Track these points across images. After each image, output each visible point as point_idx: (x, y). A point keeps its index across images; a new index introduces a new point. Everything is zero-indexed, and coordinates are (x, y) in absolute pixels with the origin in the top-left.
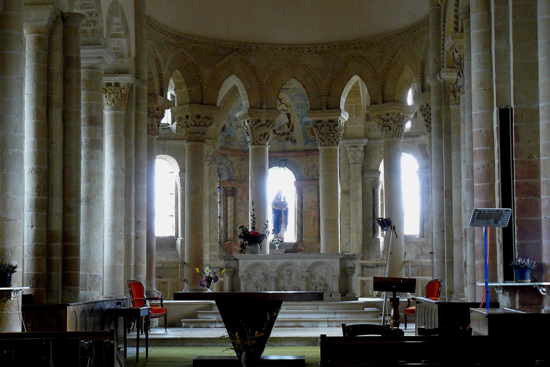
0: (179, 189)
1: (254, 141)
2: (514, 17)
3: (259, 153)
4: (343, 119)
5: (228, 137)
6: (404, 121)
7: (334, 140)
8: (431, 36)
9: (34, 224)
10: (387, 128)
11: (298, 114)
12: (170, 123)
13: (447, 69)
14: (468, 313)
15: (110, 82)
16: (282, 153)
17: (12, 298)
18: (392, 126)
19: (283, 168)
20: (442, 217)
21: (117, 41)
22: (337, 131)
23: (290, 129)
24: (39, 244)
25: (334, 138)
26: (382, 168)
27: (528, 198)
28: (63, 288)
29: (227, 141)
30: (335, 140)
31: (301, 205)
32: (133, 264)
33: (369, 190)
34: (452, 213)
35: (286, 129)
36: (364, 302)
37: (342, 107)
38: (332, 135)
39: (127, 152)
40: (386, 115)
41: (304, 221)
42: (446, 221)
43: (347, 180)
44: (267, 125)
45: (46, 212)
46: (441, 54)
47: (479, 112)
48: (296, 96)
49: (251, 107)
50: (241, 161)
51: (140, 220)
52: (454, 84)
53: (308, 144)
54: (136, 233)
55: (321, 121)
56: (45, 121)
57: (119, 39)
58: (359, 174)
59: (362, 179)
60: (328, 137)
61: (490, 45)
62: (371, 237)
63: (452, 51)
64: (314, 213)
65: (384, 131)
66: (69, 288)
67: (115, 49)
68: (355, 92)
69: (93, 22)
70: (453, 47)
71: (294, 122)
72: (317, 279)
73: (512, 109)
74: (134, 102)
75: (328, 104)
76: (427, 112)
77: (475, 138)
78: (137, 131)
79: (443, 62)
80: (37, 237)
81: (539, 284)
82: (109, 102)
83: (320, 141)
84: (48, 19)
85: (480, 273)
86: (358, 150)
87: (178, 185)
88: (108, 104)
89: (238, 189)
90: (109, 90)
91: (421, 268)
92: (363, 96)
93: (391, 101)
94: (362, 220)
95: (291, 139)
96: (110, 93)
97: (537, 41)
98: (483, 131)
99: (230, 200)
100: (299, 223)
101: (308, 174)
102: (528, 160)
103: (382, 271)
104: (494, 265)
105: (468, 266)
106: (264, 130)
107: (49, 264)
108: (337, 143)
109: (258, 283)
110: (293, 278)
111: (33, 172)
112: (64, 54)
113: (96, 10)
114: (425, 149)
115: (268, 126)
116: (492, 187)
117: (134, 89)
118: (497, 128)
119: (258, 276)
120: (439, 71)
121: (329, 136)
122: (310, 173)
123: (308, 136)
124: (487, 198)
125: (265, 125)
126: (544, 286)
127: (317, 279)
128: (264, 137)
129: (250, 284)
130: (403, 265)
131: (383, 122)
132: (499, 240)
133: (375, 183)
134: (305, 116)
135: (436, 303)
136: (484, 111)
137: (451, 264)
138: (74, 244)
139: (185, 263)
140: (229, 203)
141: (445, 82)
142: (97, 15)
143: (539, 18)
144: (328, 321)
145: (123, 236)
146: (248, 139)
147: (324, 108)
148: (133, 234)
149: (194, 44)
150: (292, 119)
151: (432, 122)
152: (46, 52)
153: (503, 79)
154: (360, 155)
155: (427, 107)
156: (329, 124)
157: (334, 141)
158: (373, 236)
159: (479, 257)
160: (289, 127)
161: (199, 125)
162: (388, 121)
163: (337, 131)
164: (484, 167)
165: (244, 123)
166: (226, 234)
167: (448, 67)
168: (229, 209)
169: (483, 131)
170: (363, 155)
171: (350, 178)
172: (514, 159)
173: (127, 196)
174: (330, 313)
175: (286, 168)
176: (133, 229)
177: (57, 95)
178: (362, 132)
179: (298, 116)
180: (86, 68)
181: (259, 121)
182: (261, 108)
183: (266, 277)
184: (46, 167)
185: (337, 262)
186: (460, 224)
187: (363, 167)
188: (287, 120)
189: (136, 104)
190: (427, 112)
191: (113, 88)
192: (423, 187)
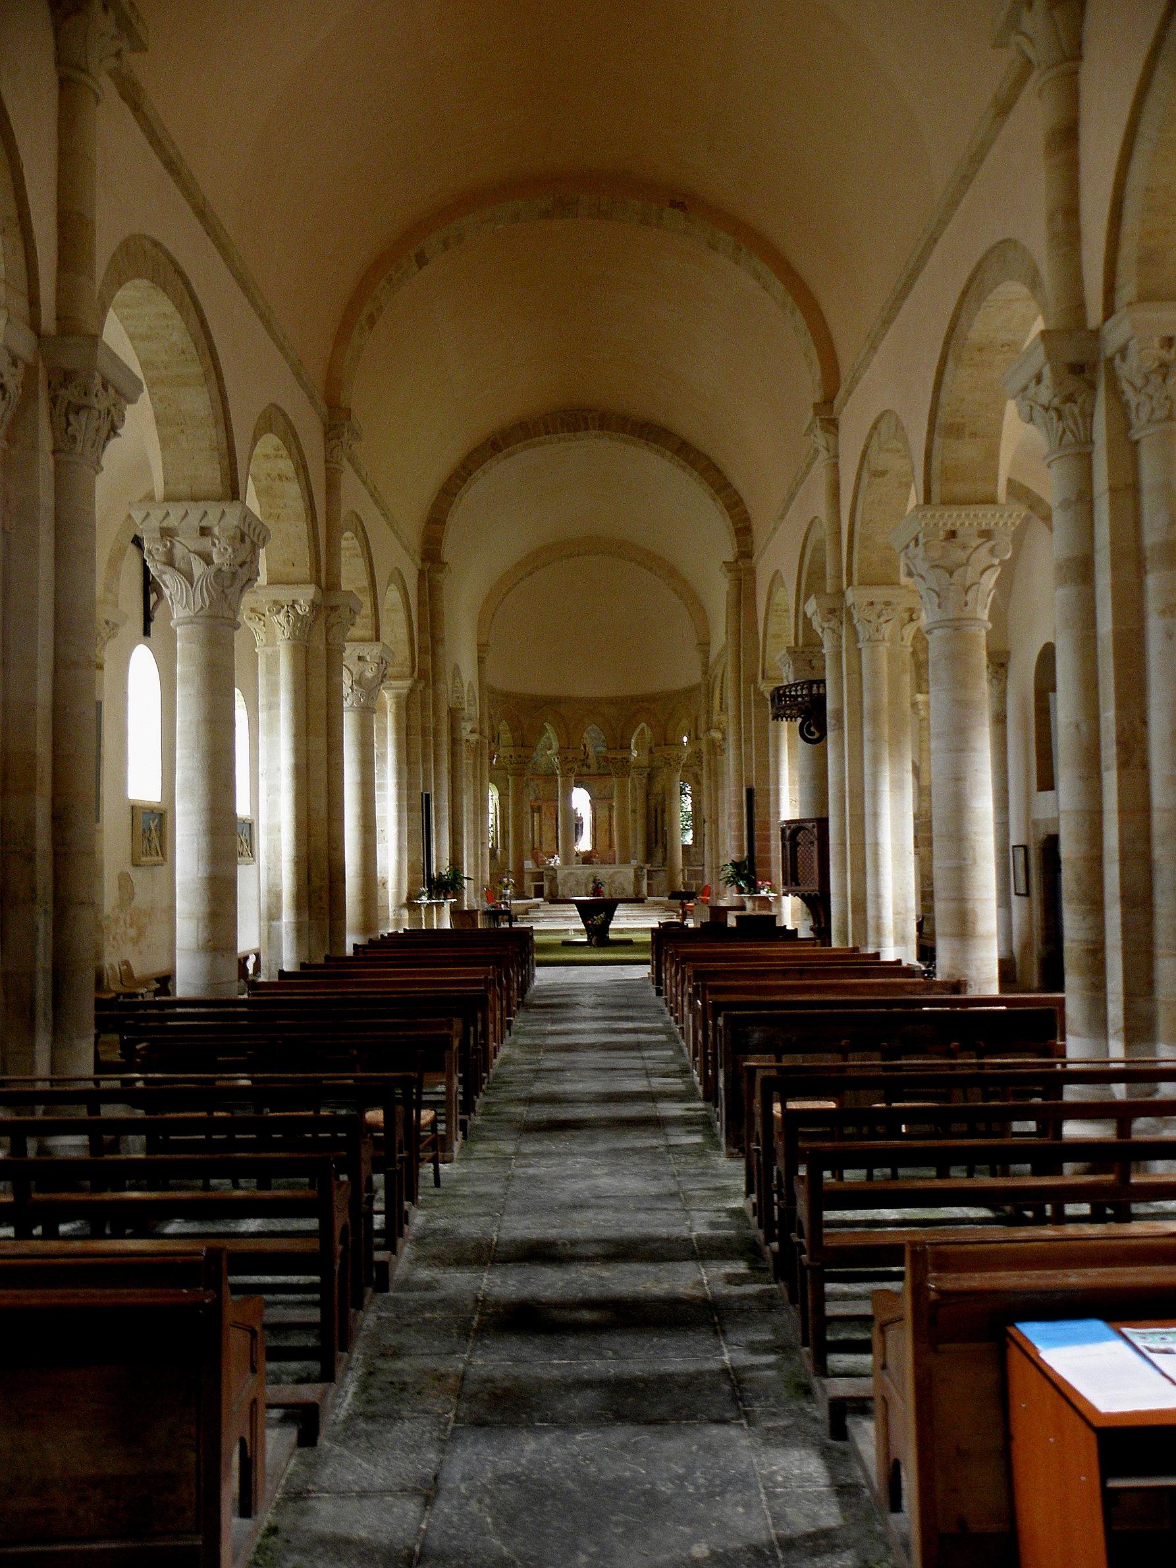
31: (594, 819)
49: (561, 748)
68: (642, 730)
78: (481, 773)
120: (708, 730)
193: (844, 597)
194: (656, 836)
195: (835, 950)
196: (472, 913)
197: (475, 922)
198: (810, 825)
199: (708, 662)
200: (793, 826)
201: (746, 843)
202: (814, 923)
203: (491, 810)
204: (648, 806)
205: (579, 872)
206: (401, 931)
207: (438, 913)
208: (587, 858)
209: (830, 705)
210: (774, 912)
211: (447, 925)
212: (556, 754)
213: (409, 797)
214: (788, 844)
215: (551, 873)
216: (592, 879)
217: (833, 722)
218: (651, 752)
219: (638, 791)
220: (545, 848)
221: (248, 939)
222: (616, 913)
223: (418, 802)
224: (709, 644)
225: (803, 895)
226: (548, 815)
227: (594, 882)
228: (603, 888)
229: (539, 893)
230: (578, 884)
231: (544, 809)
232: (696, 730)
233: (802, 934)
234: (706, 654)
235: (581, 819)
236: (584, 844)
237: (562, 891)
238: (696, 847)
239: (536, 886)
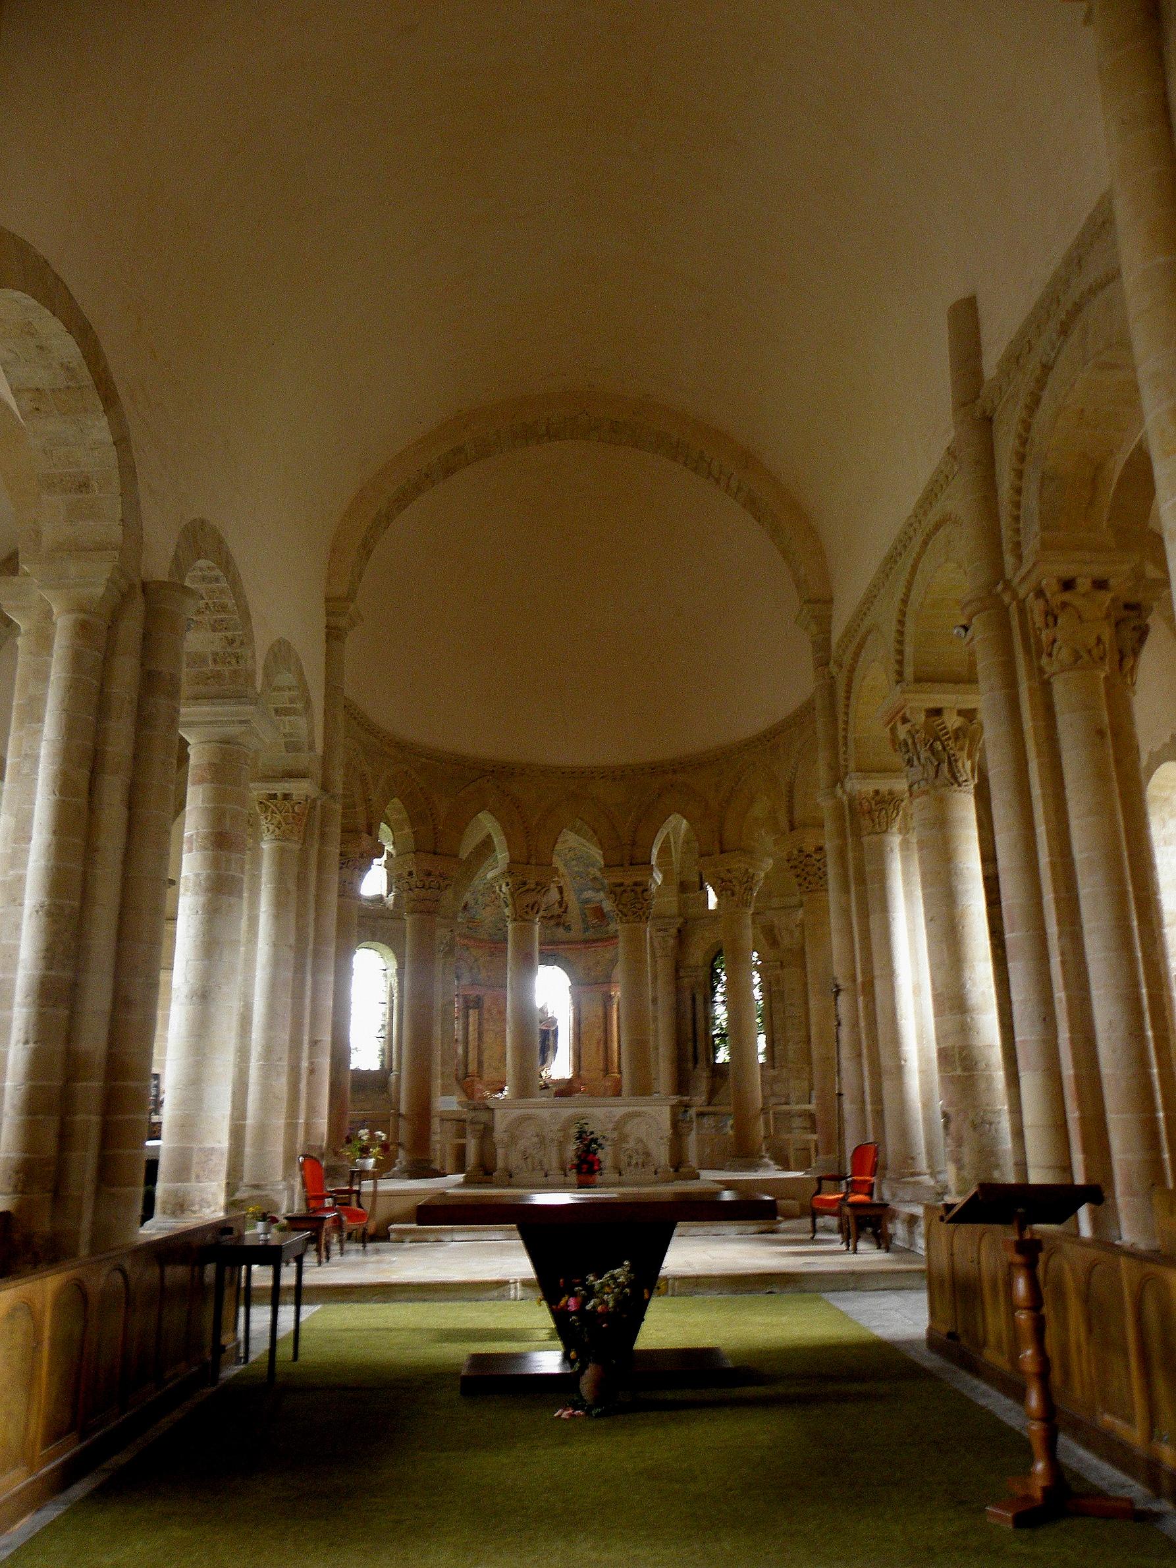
0: (396, 995)
1: (516, 914)
3: (524, 936)
5: (472, 919)
8: (820, 723)
9: (31, 1035)
12: (384, 893)
15: (273, 792)
18: (737, 888)
21: (289, 721)
24: (40, 1083)
28: (98, 1192)
30: (644, 913)
31: (578, 1022)
32: (302, 1121)
35: (557, 910)
37: (653, 862)
38: (639, 906)
39: (300, 916)
45: (66, 1008)
48: (573, 860)
49: (512, 862)
54: (311, 1063)
55: (621, 885)
56: (82, 801)
57: (292, 718)
64: (599, 1033)
66: (113, 1190)
67: (285, 735)
69: (235, 657)
72: (631, 1144)
74: (317, 832)
80: (38, 1067)
82: (272, 828)
84: (105, 582)
88: (268, 831)
90: (272, 806)
96: (273, 812)
99: (473, 1015)
105: (1030, 1126)
107: (65, 1137)
108: (647, 918)
111: (41, 913)
112: (142, 665)
113: (240, 633)
117: (319, 809)
119: (527, 1141)
121: (634, 907)
127: (631, 1144)
128: (532, 909)
138: (131, 1084)
139: (400, 1115)
140: (471, 1019)
141: (851, 800)
142: (242, 643)
145: (286, 1069)
146: (507, 911)
147: (626, 863)
148: (305, 1064)
149: (424, 760)
150: (565, 894)
152: (100, 656)
160: (560, 907)
161: (430, 888)
165: (500, 887)
166: (466, 1066)
167: (859, 770)
168: (471, 1028)
173: (298, 997)
175: (555, 967)
177: (119, 745)
180: (221, 742)
181: (524, 884)
183: (542, 1141)
184: (76, 904)
188: (558, 897)
189: (321, 834)
191: (279, 802)
194: (695, 1048)
199: (828, 640)
204: (678, 990)
205: (545, 1114)
208: (565, 1090)
212: (503, 875)
215: (483, 1116)
216: (574, 1131)
219: (660, 962)
220: (489, 1074)
221: (296, 1207)
224: (830, 601)
227: (581, 1135)
228: (600, 1154)
234: (824, 623)
235: (553, 1021)
236: (560, 1067)
238: (774, 1067)
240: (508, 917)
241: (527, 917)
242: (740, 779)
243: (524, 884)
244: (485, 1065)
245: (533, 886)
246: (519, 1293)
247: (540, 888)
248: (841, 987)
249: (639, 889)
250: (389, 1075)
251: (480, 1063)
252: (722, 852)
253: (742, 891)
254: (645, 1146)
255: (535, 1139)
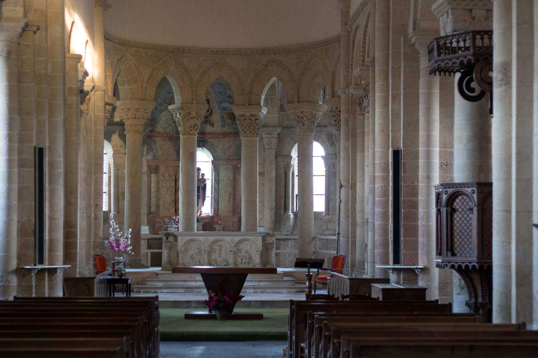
0: (112, 169)
1: (185, 130)
2: (404, 89)
4: (263, 113)
6: (316, 118)
7: (254, 132)
10: (302, 124)
11: (216, 100)
13: (355, 86)
14: (370, 287)
16: (201, 135)
17: (316, 293)
18: (306, 122)
19: (202, 148)
20: (348, 205)
22: (257, 125)
23: (209, 113)
25: (255, 130)
26: (294, 154)
27: (410, 210)
29: (152, 124)
31: (217, 181)
33: (282, 171)
34: (356, 202)
36: (282, 273)
37: (262, 104)
38: (253, 128)
40: (300, 113)
41: (220, 196)
42: (351, 209)
43: (263, 162)
44: (196, 118)
46: (350, 72)
47: (380, 150)
50: (163, 141)
51: (98, 203)
52: (360, 99)
53: (225, 127)
54: (95, 215)
55: (243, 115)
58: (275, 158)
59: (276, 162)
60: (250, 130)
61: (388, 104)
62: (283, 214)
63: (360, 78)
65: (298, 126)
68: (273, 86)
70: (360, 76)
71: (213, 107)
73: (401, 150)
75: (250, 101)
76: (337, 114)
77: (377, 167)
79: (352, 79)
81: (415, 267)
83: (242, 132)
85: (377, 259)
86: (273, 137)
87: (111, 165)
89: (161, 167)
91: (326, 242)
92: (278, 89)
93: (305, 102)
94: (275, 199)
95: (210, 122)
97: (419, 106)
98: (382, 163)
100: (216, 198)
101: (224, 154)
102: (411, 185)
103: (292, 244)
104: (387, 254)
106: (193, 122)
108: (258, 134)
109: (194, 256)
110: (223, 252)
114: (332, 138)
115: (197, 119)
116: (387, 200)
118: (392, 162)
119: (193, 250)
120: (348, 86)
122: (227, 153)
123: (226, 119)
124: (383, 209)
125: (195, 118)
126: (418, 268)
127: (243, 253)
128: (194, 128)
129: (187, 256)
130: (312, 240)
131: (298, 118)
132: (391, 237)
133: (288, 166)
134: (223, 102)
135: (348, 278)
136: (383, 149)
137: (354, 243)
143: (420, 91)
144: (254, 288)
148: (93, 215)
151: (342, 127)
153: (395, 130)
154: (274, 141)
155: (336, 110)
156: (251, 118)
157: (255, 133)
158: (284, 213)
159: (377, 248)
161: (139, 118)
162: (302, 118)
163: (257, 125)
164: (382, 187)
168: (153, 185)
169: (382, 163)
170: (277, 140)
171: (265, 162)
172: (402, 184)
174: (256, 281)
175: (204, 148)
176: (93, 211)
178: (276, 121)
179: (217, 102)
182: (192, 103)
185: (260, 238)
186: (363, 211)
187: (276, 152)
190: (337, 114)
192: (329, 171)
193: (105, 37)
195: (498, 326)
196: (87, 282)
197: (90, 291)
198: (469, 190)
199: (348, 12)
200: (450, 191)
201: (391, 210)
202: (470, 298)
203: (106, 169)
206: (11, 299)
207: (50, 281)
209: (497, 59)
210: (421, 284)
211: (60, 294)
212: (178, 109)
213: (20, 152)
214: (444, 210)
217: (500, 76)
218: (282, 108)
220: (163, 212)
222: (246, 284)
223: (30, 156)
225: (460, 266)
226: (166, 175)
229: (156, 261)
230: (200, 252)
231: (162, 170)
232: (333, 86)
233: (457, 309)
236: (207, 209)
237: (184, 261)
239: (152, 253)
240: (180, 131)
241: (191, 133)
242: (309, 63)
243: (190, 113)
244: (161, 207)
245: (195, 115)
246: (195, 306)
247: (198, 116)
248: (343, 185)
249: (253, 119)
250: (109, 214)
251: (158, 206)
252: (298, 102)
253: (309, 123)
254: (250, 255)
255: (197, 251)
